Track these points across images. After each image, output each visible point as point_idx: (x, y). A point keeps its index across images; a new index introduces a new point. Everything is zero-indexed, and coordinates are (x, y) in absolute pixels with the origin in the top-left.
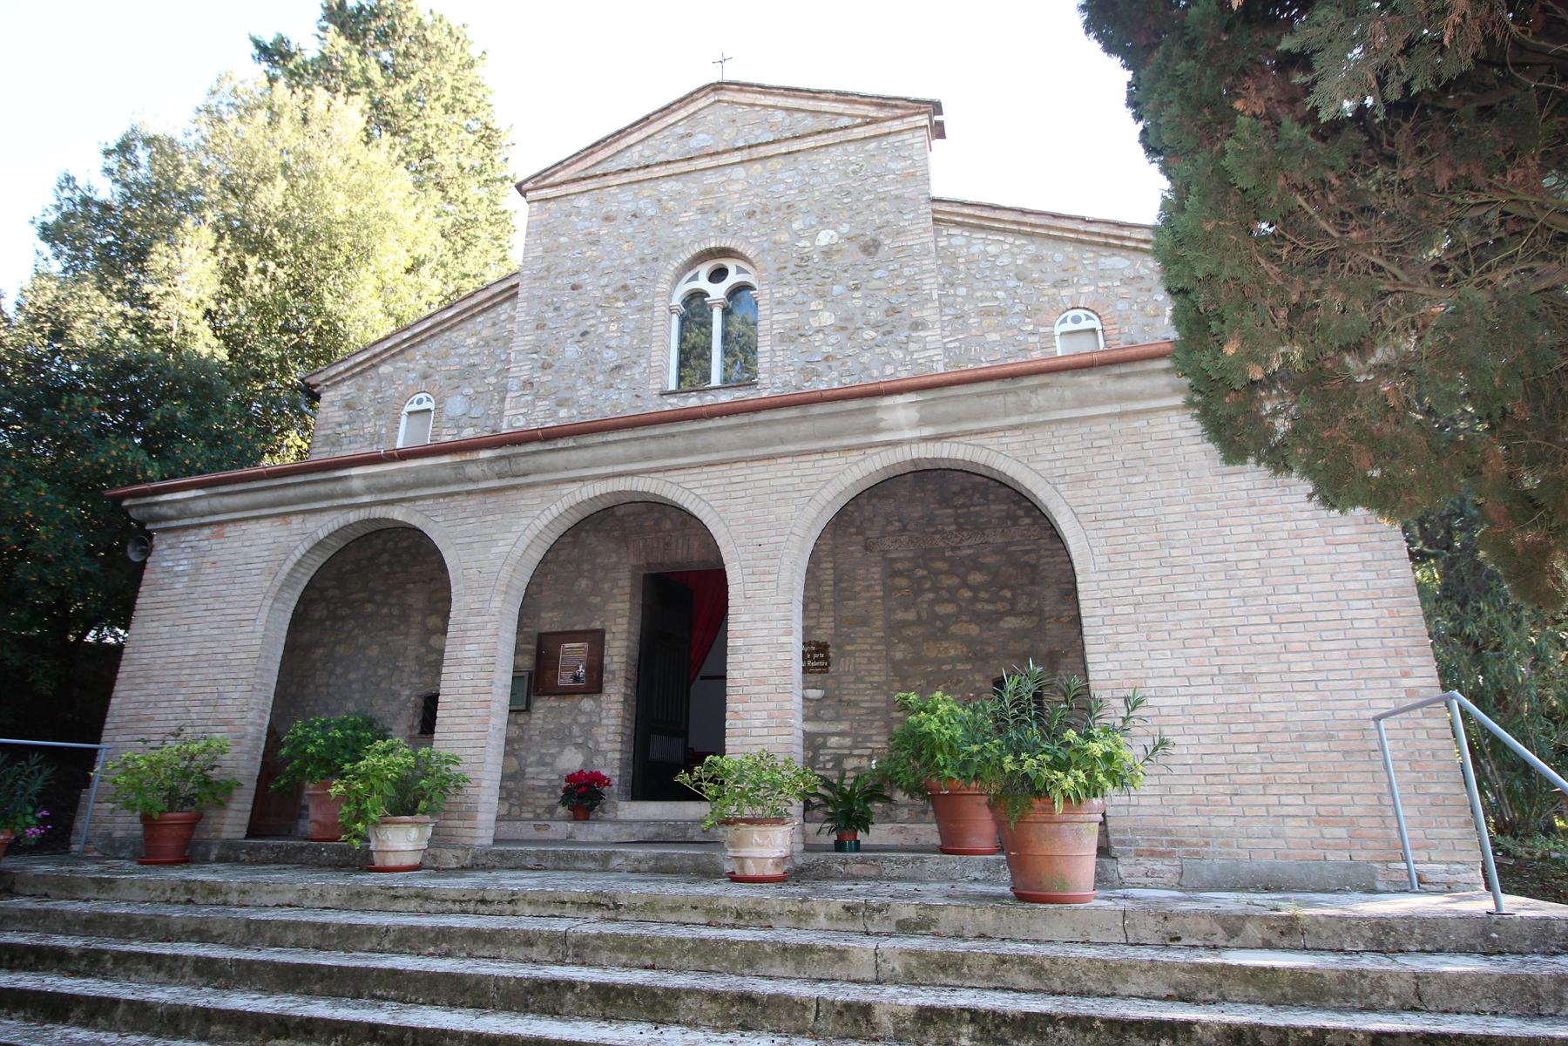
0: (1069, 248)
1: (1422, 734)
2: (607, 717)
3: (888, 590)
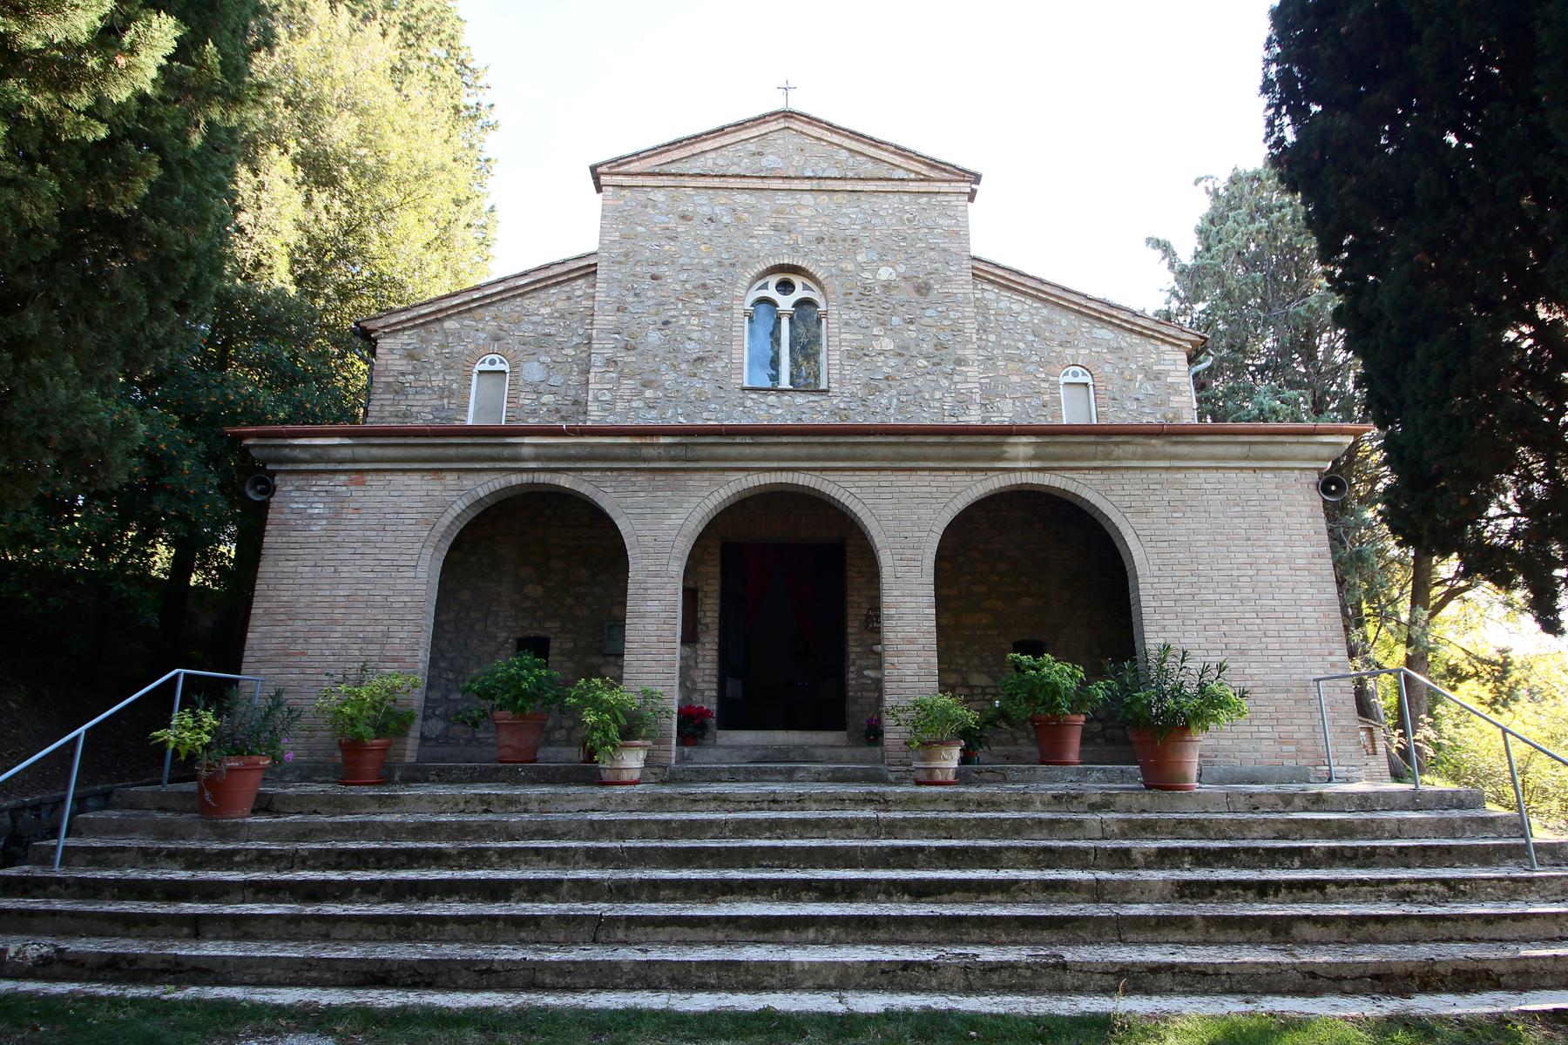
0: (1072, 317)
1: (1337, 690)
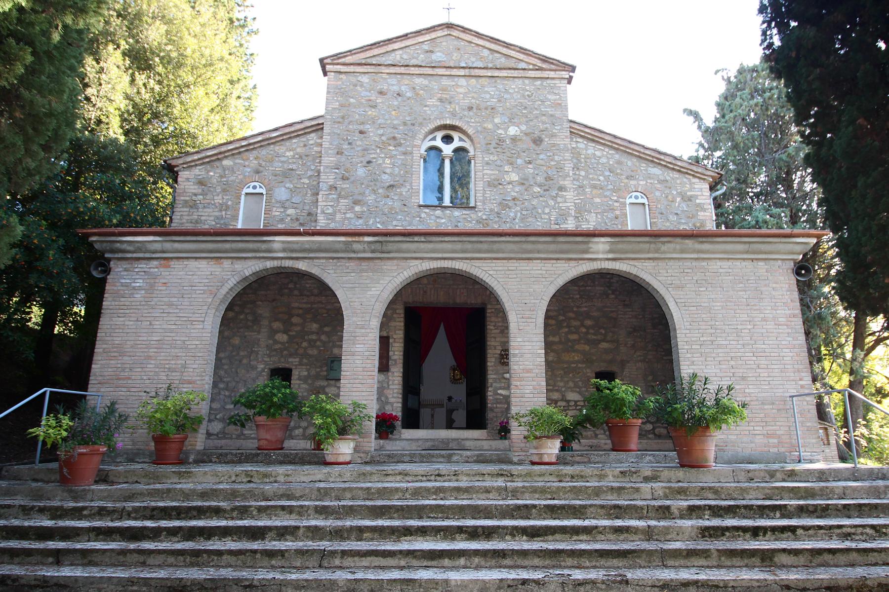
1: (805, 403)
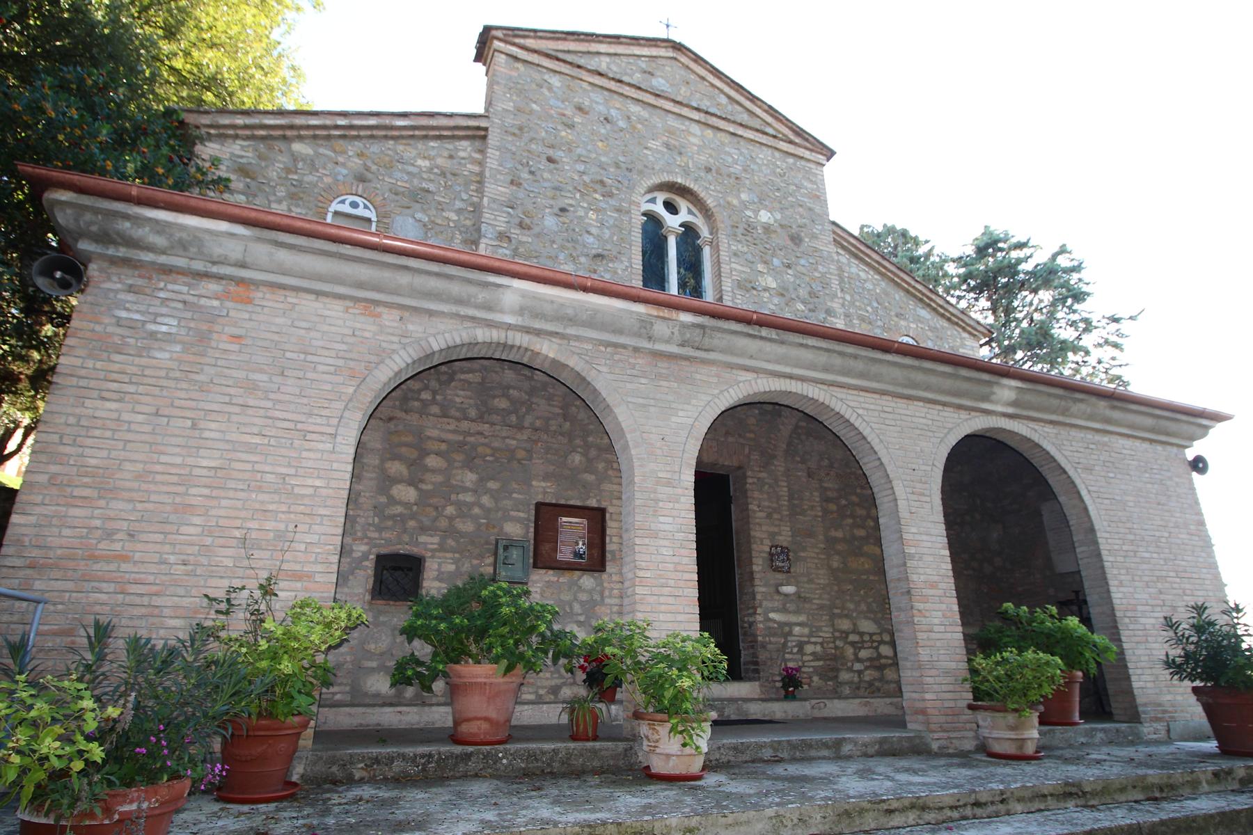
2: (610, 597)
3: (826, 512)
